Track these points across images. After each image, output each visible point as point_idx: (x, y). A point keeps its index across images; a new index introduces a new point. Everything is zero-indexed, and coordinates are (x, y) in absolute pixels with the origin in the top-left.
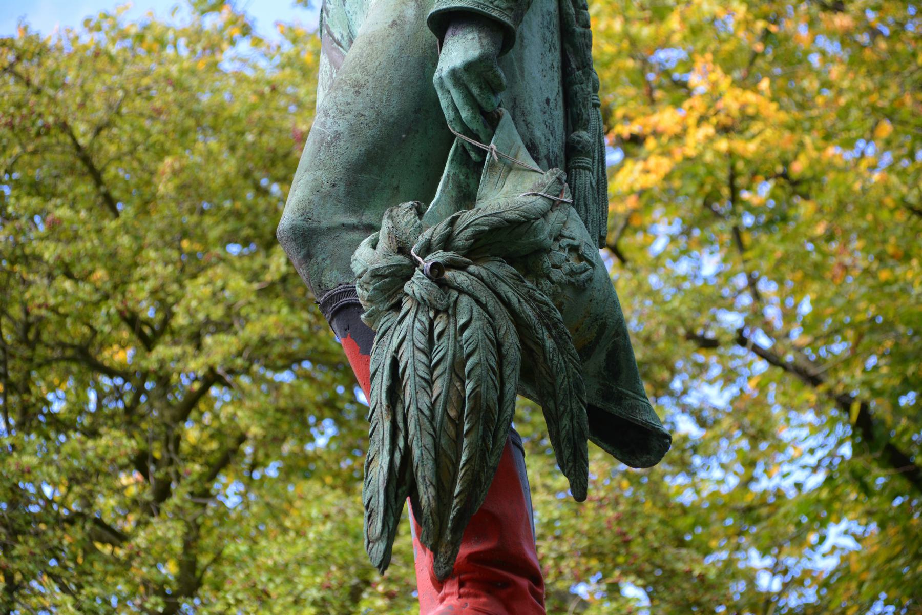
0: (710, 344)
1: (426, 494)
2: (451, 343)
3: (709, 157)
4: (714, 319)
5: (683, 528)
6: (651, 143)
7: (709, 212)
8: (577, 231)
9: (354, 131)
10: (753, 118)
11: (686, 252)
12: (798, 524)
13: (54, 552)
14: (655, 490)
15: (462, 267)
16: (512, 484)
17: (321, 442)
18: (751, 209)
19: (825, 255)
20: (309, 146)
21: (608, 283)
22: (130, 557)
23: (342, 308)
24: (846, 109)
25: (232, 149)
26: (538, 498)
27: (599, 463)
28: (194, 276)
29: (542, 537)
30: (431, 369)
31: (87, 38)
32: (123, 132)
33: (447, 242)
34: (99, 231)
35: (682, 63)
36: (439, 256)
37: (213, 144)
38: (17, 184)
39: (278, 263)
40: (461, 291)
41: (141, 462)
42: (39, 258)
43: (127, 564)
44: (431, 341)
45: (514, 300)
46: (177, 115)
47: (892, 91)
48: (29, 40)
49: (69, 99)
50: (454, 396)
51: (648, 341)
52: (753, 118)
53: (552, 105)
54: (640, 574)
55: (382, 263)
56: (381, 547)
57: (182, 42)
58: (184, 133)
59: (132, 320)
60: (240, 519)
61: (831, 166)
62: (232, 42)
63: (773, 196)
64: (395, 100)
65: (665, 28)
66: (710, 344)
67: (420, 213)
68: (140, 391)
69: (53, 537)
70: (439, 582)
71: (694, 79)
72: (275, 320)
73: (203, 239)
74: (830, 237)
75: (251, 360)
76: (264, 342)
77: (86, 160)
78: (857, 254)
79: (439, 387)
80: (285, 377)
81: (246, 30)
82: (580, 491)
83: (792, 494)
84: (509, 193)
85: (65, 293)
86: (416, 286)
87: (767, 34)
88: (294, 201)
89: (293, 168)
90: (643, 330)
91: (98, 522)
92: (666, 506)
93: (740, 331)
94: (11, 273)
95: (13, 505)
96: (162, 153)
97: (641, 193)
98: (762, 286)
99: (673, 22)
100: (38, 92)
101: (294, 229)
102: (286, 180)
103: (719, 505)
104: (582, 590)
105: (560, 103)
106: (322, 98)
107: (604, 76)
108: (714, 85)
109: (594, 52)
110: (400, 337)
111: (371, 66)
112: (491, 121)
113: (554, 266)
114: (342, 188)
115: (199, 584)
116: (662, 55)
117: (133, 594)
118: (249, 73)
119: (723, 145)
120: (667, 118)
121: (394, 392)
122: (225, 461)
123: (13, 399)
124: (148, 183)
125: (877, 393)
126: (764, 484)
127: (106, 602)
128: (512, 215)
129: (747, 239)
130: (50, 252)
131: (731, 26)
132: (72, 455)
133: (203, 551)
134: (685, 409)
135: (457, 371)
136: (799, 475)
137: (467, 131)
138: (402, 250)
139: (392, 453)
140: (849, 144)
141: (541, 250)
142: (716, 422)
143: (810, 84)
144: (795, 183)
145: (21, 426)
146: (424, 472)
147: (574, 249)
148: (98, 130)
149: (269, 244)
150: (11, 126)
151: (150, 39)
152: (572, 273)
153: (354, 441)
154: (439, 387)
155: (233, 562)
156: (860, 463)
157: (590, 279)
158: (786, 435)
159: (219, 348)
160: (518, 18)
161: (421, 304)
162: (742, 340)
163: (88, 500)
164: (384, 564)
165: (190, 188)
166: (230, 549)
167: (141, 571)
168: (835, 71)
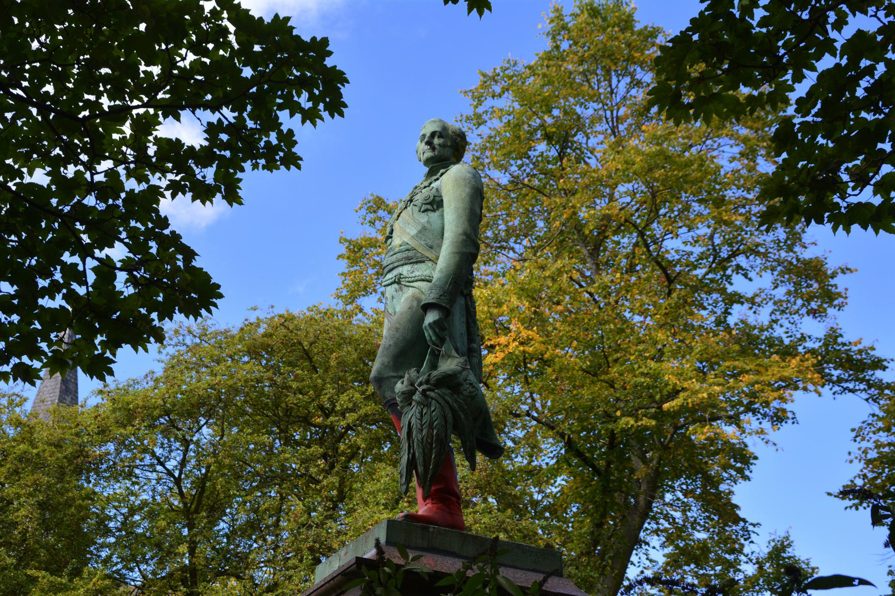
0: (517, 416)
3: (517, 352)
4: (519, 407)
5: (509, 479)
6: (497, 348)
7: (516, 372)
8: (472, 378)
9: (396, 344)
10: (531, 340)
11: (509, 384)
12: (547, 476)
13: (296, 486)
14: (499, 466)
15: (432, 390)
16: (450, 465)
17: (386, 449)
18: (531, 370)
19: (556, 386)
20: (380, 349)
21: (483, 396)
22: (321, 488)
23: (391, 405)
24: (562, 336)
25: (356, 350)
26: (459, 469)
27: (479, 457)
28: (343, 393)
29: (461, 482)
30: (422, 426)
31: (308, 314)
32: (320, 345)
33: (427, 382)
34: (311, 378)
35: (507, 321)
36: (424, 387)
37: (349, 348)
38: (284, 363)
39: (371, 389)
40: (432, 399)
41: (324, 456)
42: (291, 387)
43: (320, 491)
44: (422, 416)
46: (337, 339)
47: (576, 332)
48: (289, 315)
49: (302, 334)
50: (430, 435)
51: (497, 415)
52: (531, 340)
54: (494, 494)
55: (405, 389)
56: (405, 487)
57: (339, 315)
58: (340, 345)
59: (321, 408)
60: (358, 476)
61: (557, 356)
62: (356, 315)
63: (538, 366)
65: (501, 310)
66: (517, 416)
67: (418, 372)
68: (325, 432)
69: (295, 482)
70: (425, 499)
71: (511, 327)
72: (370, 408)
73: (345, 380)
74: (557, 379)
75: (362, 422)
76: (366, 415)
77: (307, 354)
78: (567, 386)
79: (424, 432)
80: (374, 427)
81: (361, 310)
82: (473, 467)
83: (544, 466)
84: (449, 365)
85: (299, 399)
86: (417, 397)
87: (535, 311)
88: (376, 367)
89: (375, 356)
90: (496, 410)
91: (310, 476)
92: (503, 471)
93: (528, 411)
94: (282, 392)
95: (282, 471)
96: (332, 352)
97: (495, 364)
98: (534, 395)
99: (505, 308)
100: (291, 332)
101: (375, 377)
102: (373, 361)
103: (520, 470)
104: (474, 499)
106: (385, 332)
107: (481, 325)
108: (519, 328)
109: (478, 317)
110: (411, 415)
112: (442, 341)
114: (391, 363)
115: (344, 498)
116: (500, 318)
117: (322, 501)
118: (362, 324)
119: (521, 348)
120: (503, 340)
122: (353, 456)
123: (283, 435)
124: (328, 362)
125: (573, 432)
126: (535, 463)
127: (313, 503)
128: (450, 373)
129: (530, 380)
130: (295, 385)
131: (523, 309)
132: (302, 454)
133: (346, 487)
134: (509, 438)
135: (431, 427)
136: (547, 460)
137: (434, 344)
138: (412, 384)
140: (563, 349)
141: (460, 384)
142: (519, 442)
143: (550, 329)
144: (545, 362)
145: (285, 444)
147: (471, 384)
148: (311, 344)
149: (368, 383)
150: (282, 343)
151: (328, 314)
152: (470, 392)
153: (396, 450)
154: (424, 432)
155: (356, 490)
156: (567, 456)
158: (543, 446)
159: (351, 417)
160: (452, 306)
161: (418, 403)
162: (528, 414)
163: (307, 469)
164: (407, 491)
165: (341, 363)
166: (355, 486)
167: (325, 493)
168: (558, 325)
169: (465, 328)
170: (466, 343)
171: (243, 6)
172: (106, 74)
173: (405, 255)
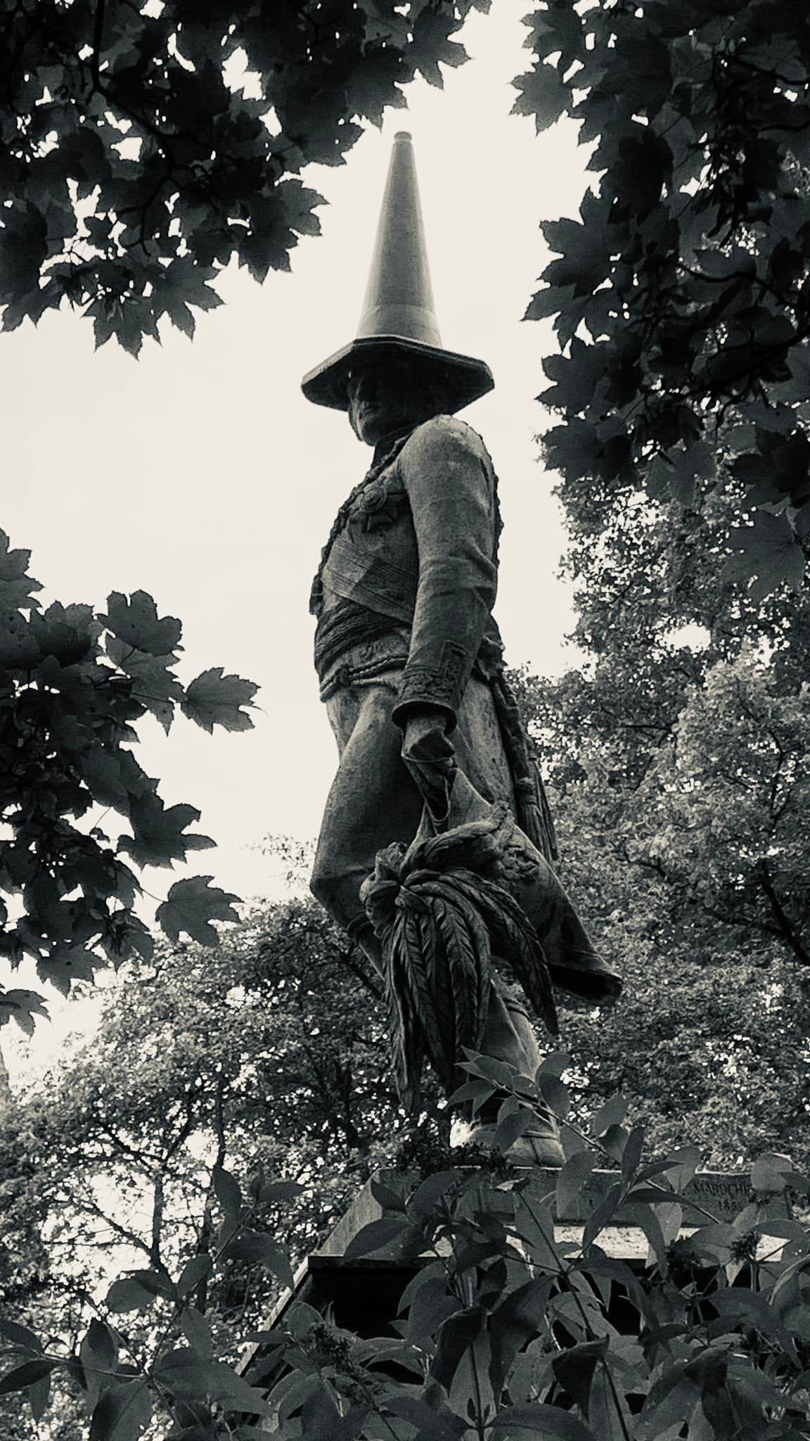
1: (437, 1049)
2: (434, 933)
9: (351, 806)
30: (422, 956)
45: (476, 894)
53: (498, 762)
64: (378, 778)
105: (504, 760)
111: (358, 758)
113: (507, 868)
121: (400, 979)
139: (406, 1024)
146: (433, 1032)
152: (521, 870)
157: (536, 873)
169: (499, 748)
170: (507, 780)
171: (49, 312)
172: (254, 64)
173: (348, 625)
